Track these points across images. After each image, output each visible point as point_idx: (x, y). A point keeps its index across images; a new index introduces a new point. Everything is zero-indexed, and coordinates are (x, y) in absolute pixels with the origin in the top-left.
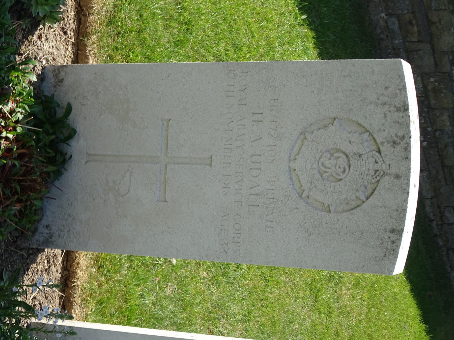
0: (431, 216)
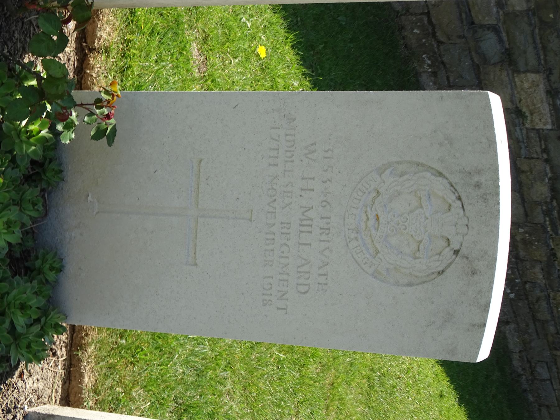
0: (520, 370)
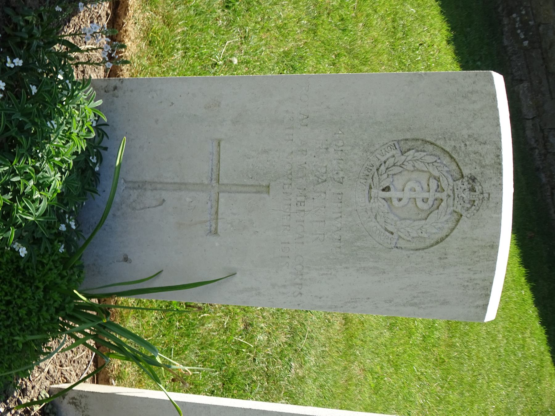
0: (533, 142)
